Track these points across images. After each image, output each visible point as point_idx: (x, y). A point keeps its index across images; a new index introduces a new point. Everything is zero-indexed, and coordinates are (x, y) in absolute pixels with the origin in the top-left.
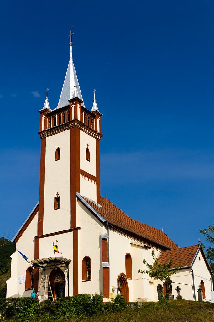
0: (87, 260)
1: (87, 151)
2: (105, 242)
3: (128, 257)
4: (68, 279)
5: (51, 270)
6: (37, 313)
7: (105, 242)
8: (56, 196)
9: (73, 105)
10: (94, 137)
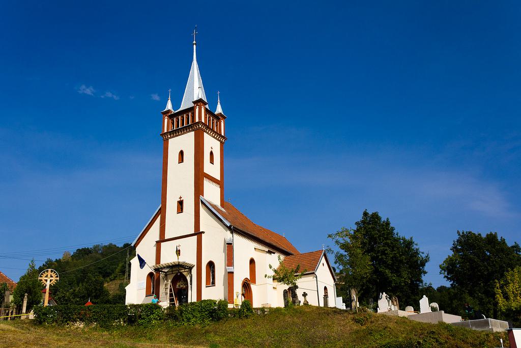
0: (211, 265)
1: (211, 153)
2: (229, 246)
3: (252, 261)
4: (191, 284)
7: (229, 246)
8: (179, 200)
9: (197, 107)
10: (218, 140)
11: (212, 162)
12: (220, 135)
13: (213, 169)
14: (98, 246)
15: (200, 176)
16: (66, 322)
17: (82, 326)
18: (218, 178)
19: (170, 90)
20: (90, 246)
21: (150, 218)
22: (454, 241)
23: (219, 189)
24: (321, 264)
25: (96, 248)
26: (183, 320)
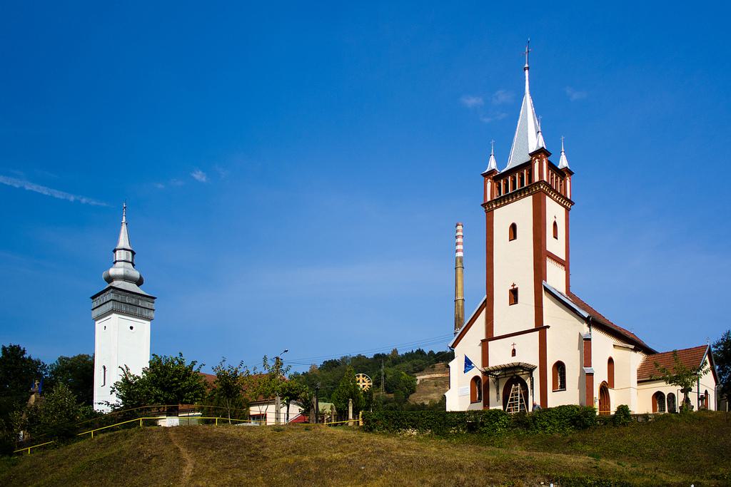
0: (560, 367)
1: (555, 224)
2: (586, 343)
3: (611, 361)
4: (532, 388)
5: (508, 379)
6: (507, 427)
7: (586, 343)
8: (512, 288)
9: (537, 160)
10: (562, 205)
11: (556, 237)
12: (566, 199)
13: (556, 246)
14: (347, 357)
15: (541, 256)
16: (398, 428)
17: (415, 433)
18: (563, 258)
19: (493, 141)
20: (337, 357)
21: (473, 311)
23: (563, 273)
25: (344, 359)
26: (537, 428)
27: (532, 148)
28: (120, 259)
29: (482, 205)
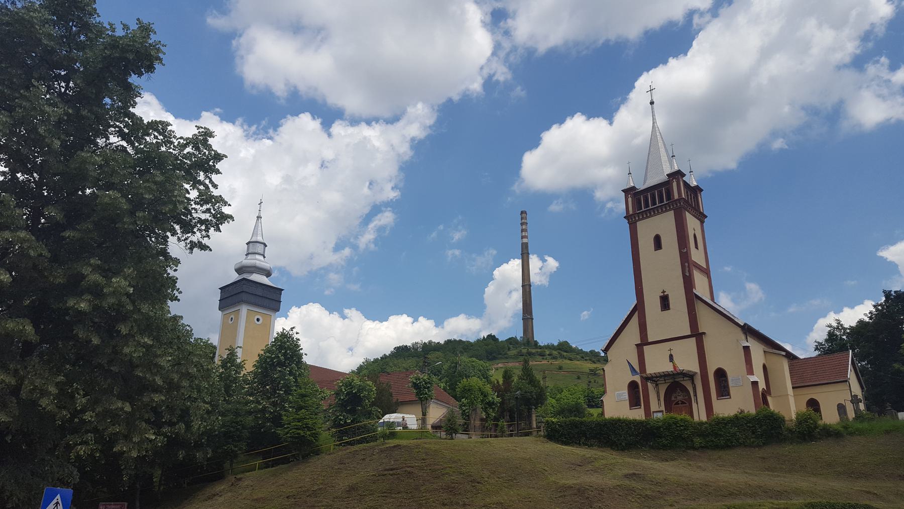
0: (721, 374)
4: (696, 395)
8: (662, 294)
9: (674, 180)
11: (697, 247)
22: (180, 293)
24: (55, 501)
27: (668, 171)
28: (262, 250)
29: (625, 217)
